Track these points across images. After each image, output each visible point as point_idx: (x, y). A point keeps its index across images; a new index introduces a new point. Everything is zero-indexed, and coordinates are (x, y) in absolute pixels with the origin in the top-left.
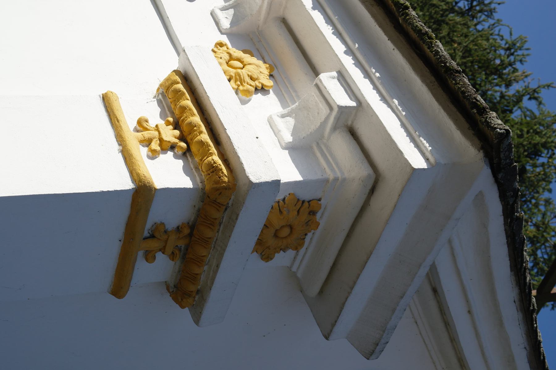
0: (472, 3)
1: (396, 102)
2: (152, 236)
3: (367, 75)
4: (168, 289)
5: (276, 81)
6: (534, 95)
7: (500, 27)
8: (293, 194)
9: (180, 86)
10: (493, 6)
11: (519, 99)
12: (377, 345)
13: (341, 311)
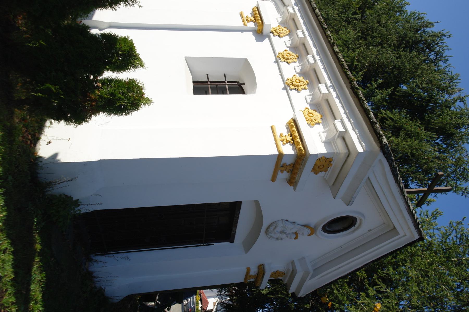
0: (437, 57)
1: (357, 130)
2: (283, 166)
3: (350, 121)
4: (287, 180)
5: (323, 120)
6: (462, 100)
7: (450, 67)
8: (324, 156)
9: (293, 124)
10: (446, 58)
11: (455, 101)
12: (350, 202)
13: (338, 191)
